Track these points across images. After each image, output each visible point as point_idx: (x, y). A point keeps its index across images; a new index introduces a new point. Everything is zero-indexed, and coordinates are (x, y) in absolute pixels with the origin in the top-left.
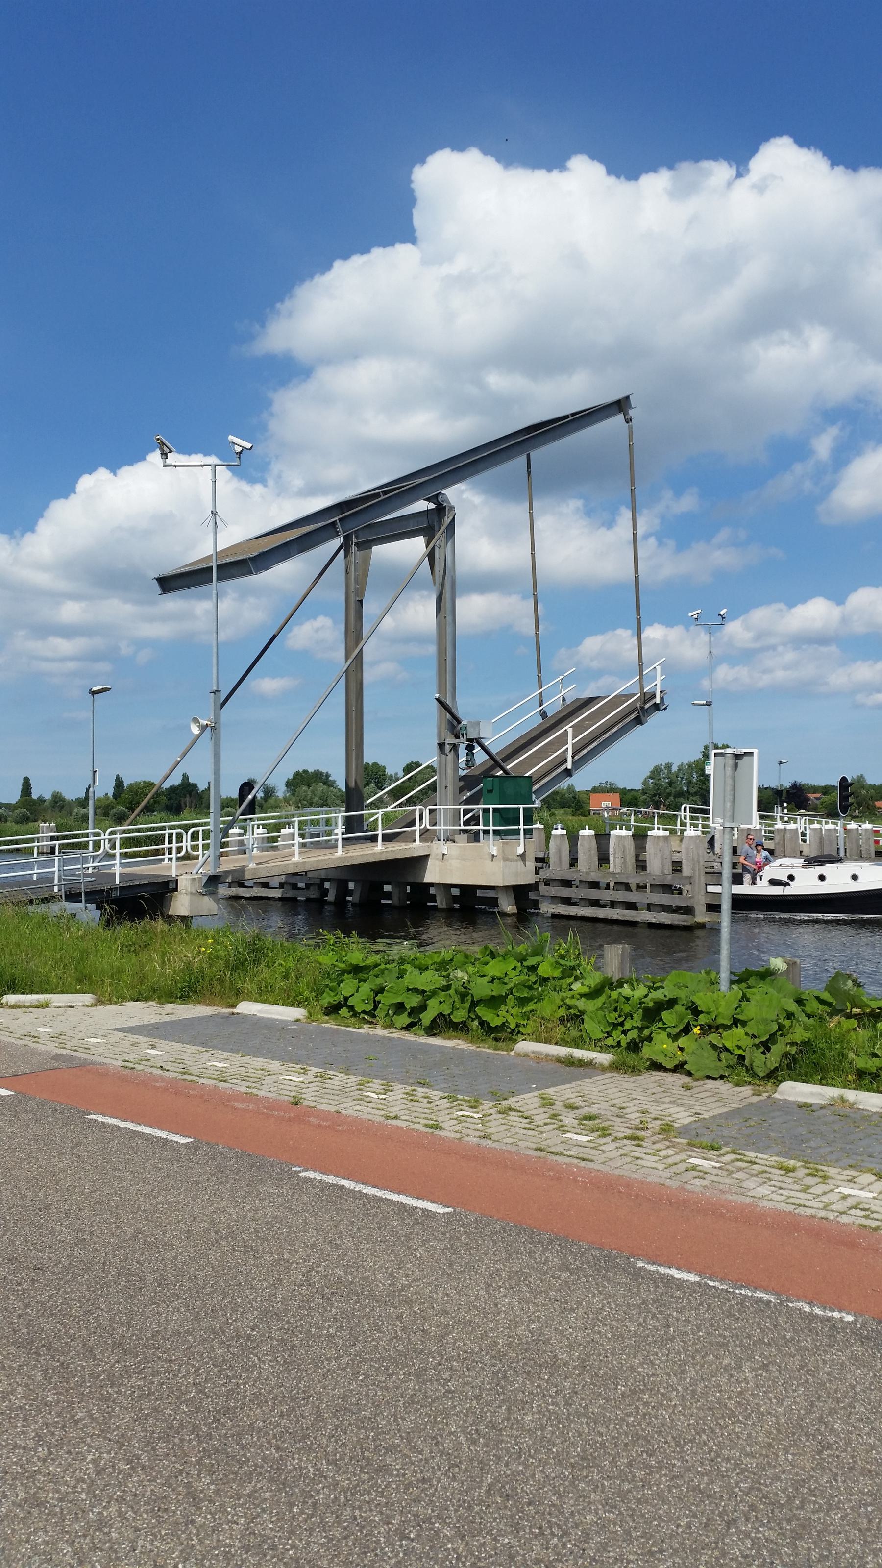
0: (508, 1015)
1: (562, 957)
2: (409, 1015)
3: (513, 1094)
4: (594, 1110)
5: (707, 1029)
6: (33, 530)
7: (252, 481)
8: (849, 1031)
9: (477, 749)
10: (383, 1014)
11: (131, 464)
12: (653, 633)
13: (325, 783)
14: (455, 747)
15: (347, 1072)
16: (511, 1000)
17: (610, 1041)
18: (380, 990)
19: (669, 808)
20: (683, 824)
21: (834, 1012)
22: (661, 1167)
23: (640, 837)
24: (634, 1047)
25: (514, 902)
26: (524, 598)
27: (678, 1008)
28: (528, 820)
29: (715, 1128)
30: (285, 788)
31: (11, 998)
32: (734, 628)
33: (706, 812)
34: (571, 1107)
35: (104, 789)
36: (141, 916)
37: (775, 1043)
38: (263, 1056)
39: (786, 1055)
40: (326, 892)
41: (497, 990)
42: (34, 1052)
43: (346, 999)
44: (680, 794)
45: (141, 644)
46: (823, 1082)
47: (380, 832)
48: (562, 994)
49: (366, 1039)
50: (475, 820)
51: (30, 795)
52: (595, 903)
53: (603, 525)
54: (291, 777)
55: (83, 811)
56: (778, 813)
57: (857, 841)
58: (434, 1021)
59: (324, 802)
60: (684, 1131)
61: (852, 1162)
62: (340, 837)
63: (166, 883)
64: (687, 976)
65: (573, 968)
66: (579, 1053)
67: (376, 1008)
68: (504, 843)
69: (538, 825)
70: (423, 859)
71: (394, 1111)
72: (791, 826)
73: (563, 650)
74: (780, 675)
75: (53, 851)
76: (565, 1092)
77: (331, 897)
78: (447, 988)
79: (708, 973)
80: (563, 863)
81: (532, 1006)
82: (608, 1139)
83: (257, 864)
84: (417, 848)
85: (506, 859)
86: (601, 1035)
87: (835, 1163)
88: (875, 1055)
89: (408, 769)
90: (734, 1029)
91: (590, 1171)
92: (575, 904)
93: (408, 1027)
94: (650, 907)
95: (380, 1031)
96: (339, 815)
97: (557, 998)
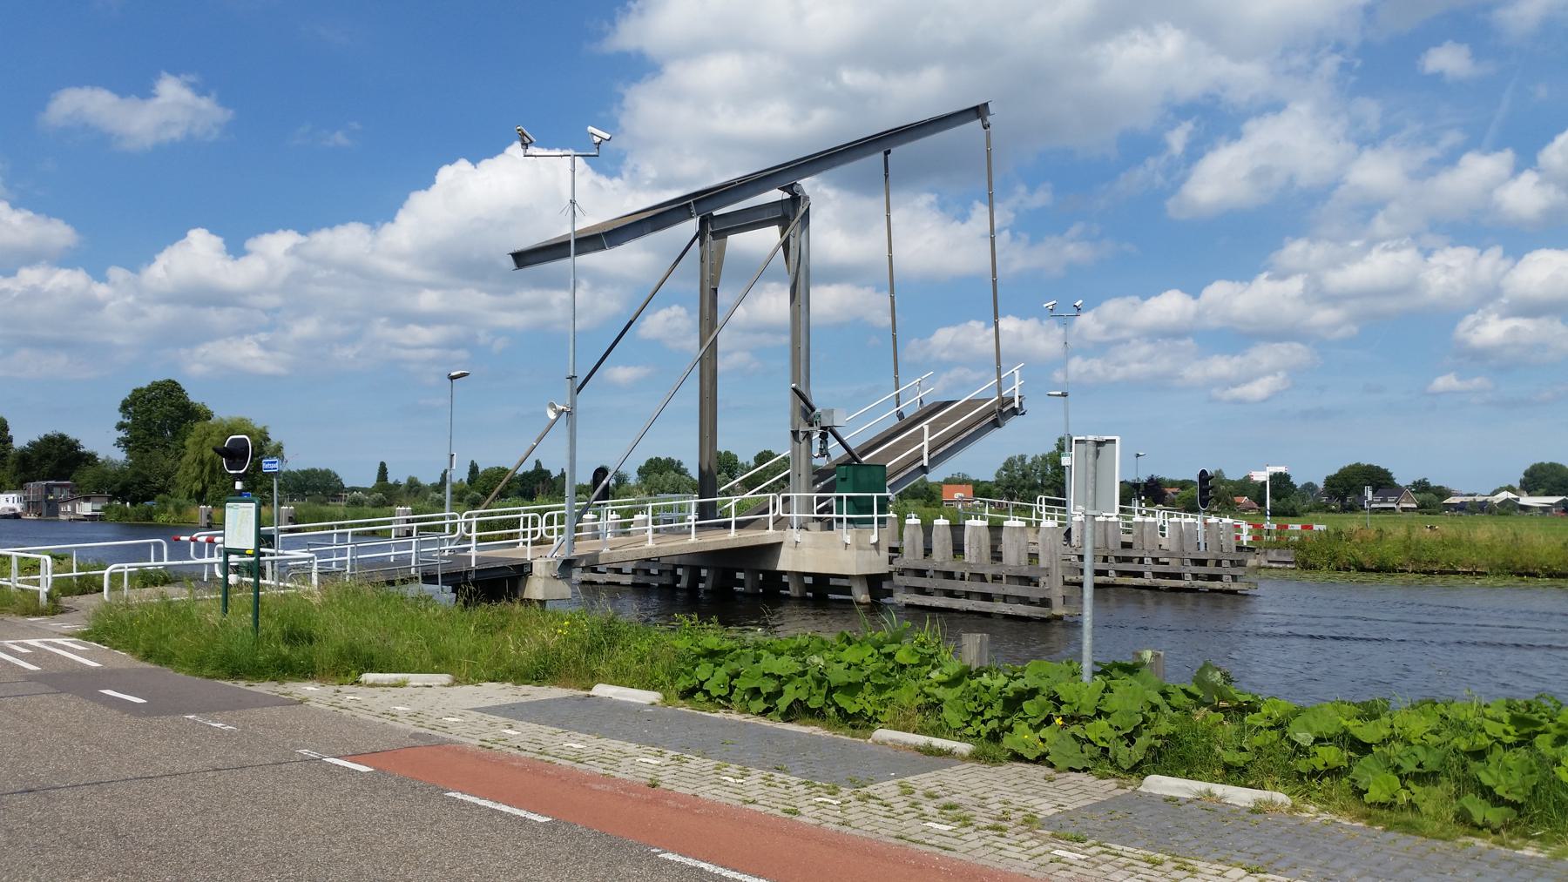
0: (864, 702)
1: (922, 645)
2: (765, 700)
3: (872, 782)
4: (955, 799)
5: (1069, 720)
6: (393, 221)
7: (611, 175)
8: (1215, 725)
9: (831, 437)
10: (738, 699)
11: (491, 157)
12: (1008, 324)
14: (808, 435)
15: (704, 755)
16: (868, 687)
17: (969, 731)
18: (736, 675)
19: (1023, 499)
20: (1039, 516)
21: (1201, 703)
22: (1025, 858)
23: (995, 528)
24: (994, 737)
26: (879, 290)
27: (1039, 698)
28: (882, 509)
29: (1079, 819)
31: (369, 677)
32: (1086, 319)
33: (1063, 504)
34: (931, 796)
35: (460, 474)
36: (498, 600)
37: (1140, 735)
38: (620, 738)
39: (1150, 748)
40: (678, 579)
41: (855, 676)
42: (393, 730)
43: (702, 683)
44: (1034, 487)
45: (498, 332)
46: (1189, 775)
47: (733, 519)
48: (921, 682)
49: (722, 724)
50: (828, 509)
52: (950, 594)
53: (956, 218)
55: (438, 496)
56: (1135, 506)
57: (1218, 536)
58: (790, 707)
59: (676, 490)
60: (1048, 822)
61: (1222, 857)
64: (1047, 666)
65: (932, 656)
66: (938, 742)
67: (731, 692)
69: (892, 514)
70: (774, 548)
71: (752, 795)
72: (1150, 519)
73: (914, 341)
74: (1135, 368)
75: (409, 534)
76: (925, 781)
77: (683, 584)
78: (804, 673)
79: (1069, 663)
81: (889, 694)
82: (970, 829)
84: (769, 535)
85: (859, 548)
86: (960, 725)
87: (1204, 857)
88: (1243, 749)
89: (763, 457)
90: (1097, 721)
91: (953, 860)
92: (929, 594)
93: (764, 713)
94: (1005, 598)
95: (735, 716)
96: (693, 501)
97: (915, 686)
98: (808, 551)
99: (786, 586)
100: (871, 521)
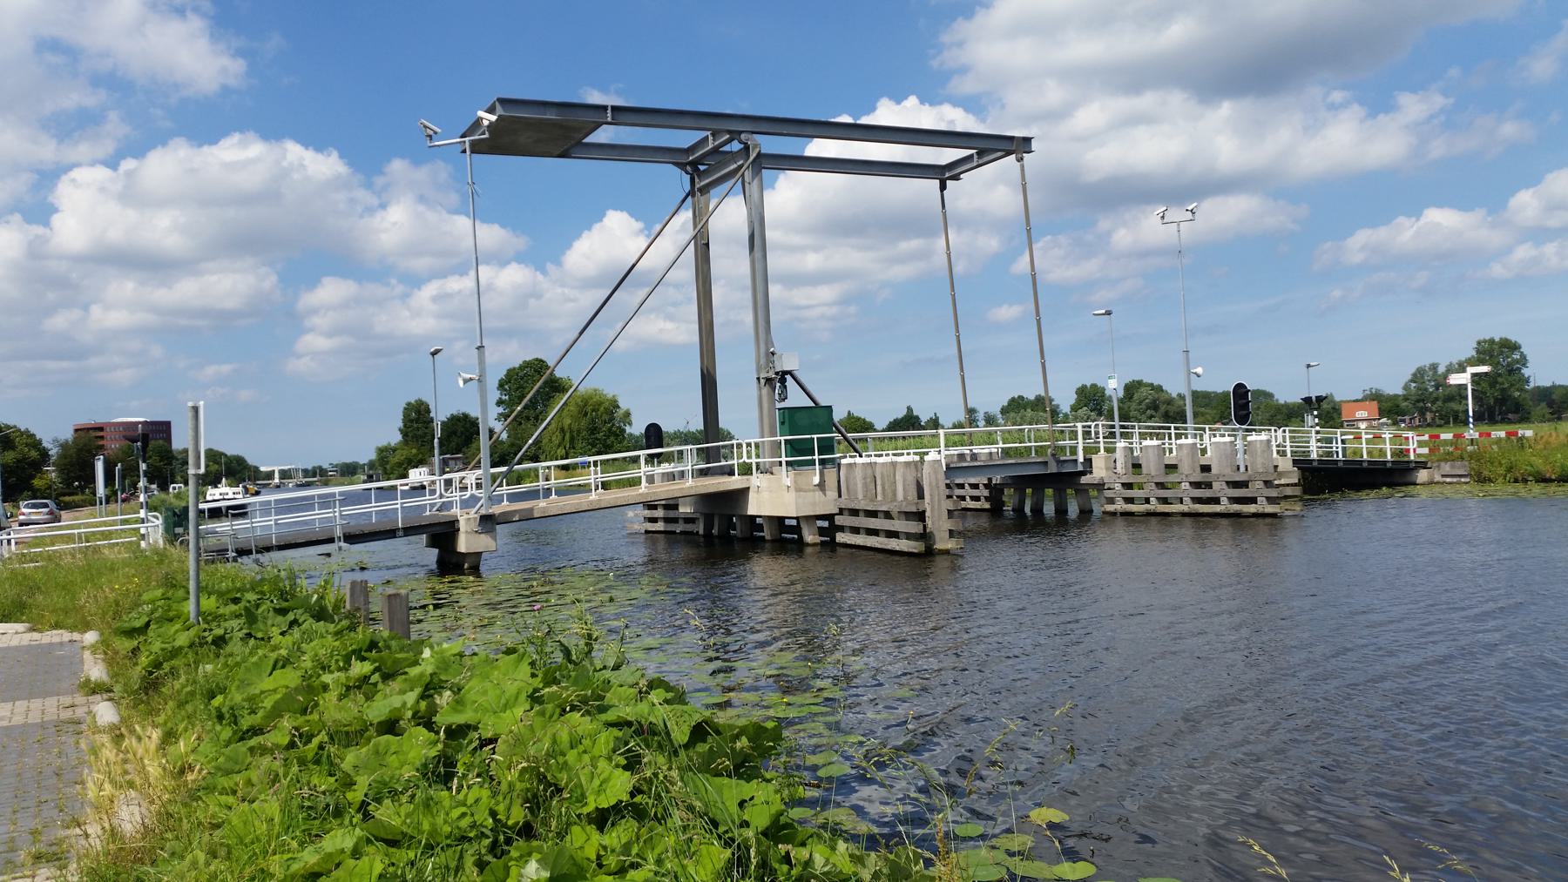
70: (744, 492)
84: (735, 482)
100: (812, 463)
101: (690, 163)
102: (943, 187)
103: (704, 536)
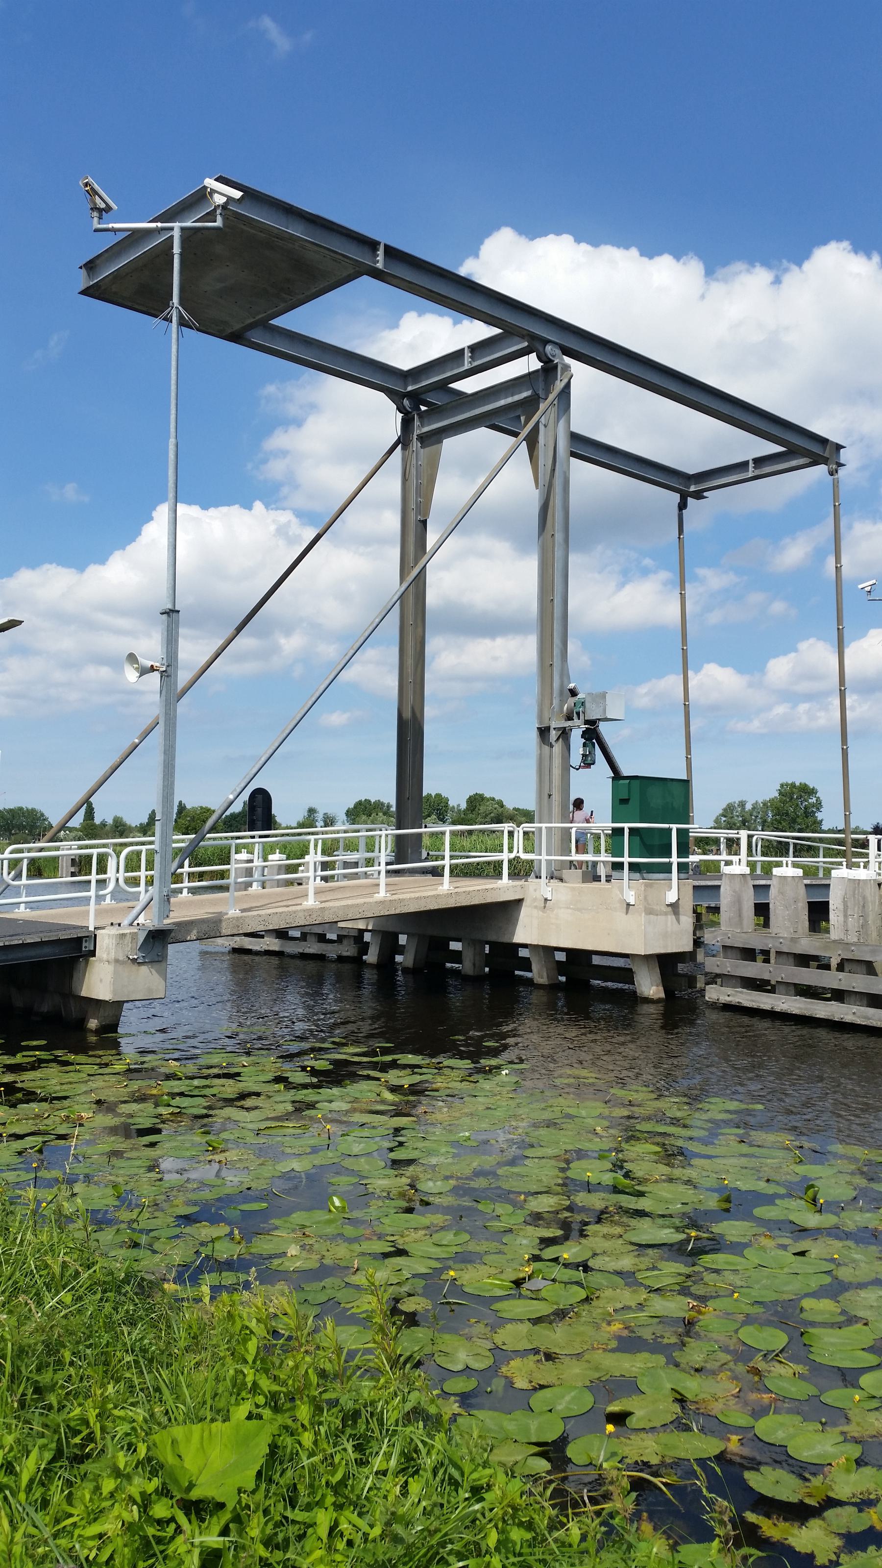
13: (385, 814)
14: (564, 734)
25: (659, 981)
30: (345, 818)
51: (93, 819)
54: (352, 806)
62: (383, 868)
63: (79, 940)
68: (646, 885)
77: (371, 957)
80: (745, 922)
83: (243, 911)
84: (503, 888)
85: (649, 912)
98: (564, 915)
99: (526, 964)
101: (410, 395)
102: (682, 506)
103: (378, 966)
